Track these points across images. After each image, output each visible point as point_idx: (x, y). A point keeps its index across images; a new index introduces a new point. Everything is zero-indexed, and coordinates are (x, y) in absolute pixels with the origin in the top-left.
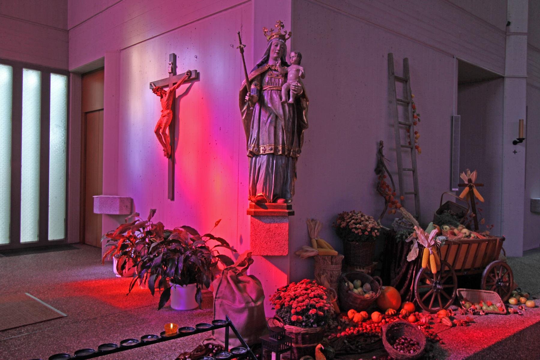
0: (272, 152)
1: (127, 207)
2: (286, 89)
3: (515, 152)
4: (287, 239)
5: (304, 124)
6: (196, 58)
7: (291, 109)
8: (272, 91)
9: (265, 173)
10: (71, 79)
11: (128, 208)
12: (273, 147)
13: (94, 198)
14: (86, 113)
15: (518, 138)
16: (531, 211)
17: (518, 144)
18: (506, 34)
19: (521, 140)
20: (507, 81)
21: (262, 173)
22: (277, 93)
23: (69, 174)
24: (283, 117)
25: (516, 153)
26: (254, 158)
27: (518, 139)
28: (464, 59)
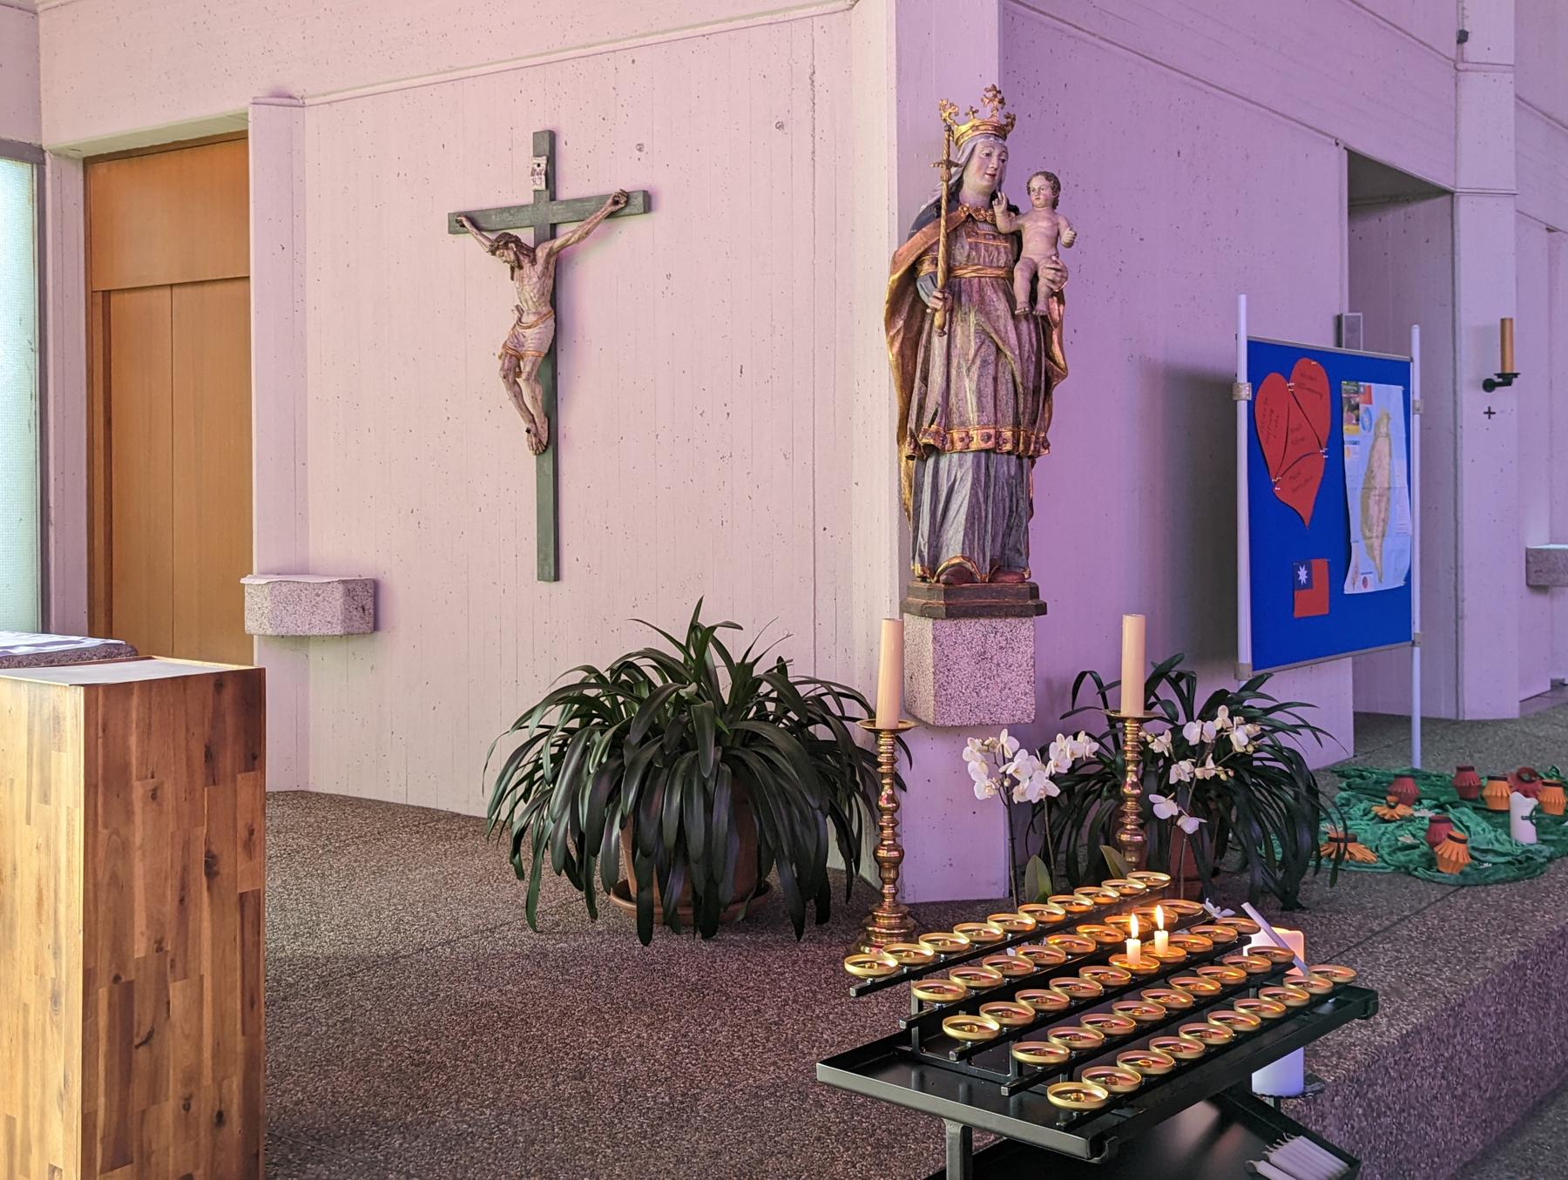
0: (990, 444)
1: (364, 610)
2: (1027, 275)
3: (1490, 413)
4: (1032, 679)
5: (1056, 368)
6: (640, 150)
7: (1032, 327)
8: (983, 279)
9: (970, 502)
10: (48, 175)
11: (367, 612)
12: (992, 432)
13: (243, 585)
14: (107, 294)
15: (1499, 372)
16: (1528, 584)
17: (1498, 389)
18: (1458, 66)
19: (1507, 379)
20: (1464, 207)
21: (959, 502)
22: (996, 286)
23: (52, 504)
24: (1017, 352)
25: (1487, 410)
26: (931, 462)
27: (1499, 376)
28: (1362, 147)
